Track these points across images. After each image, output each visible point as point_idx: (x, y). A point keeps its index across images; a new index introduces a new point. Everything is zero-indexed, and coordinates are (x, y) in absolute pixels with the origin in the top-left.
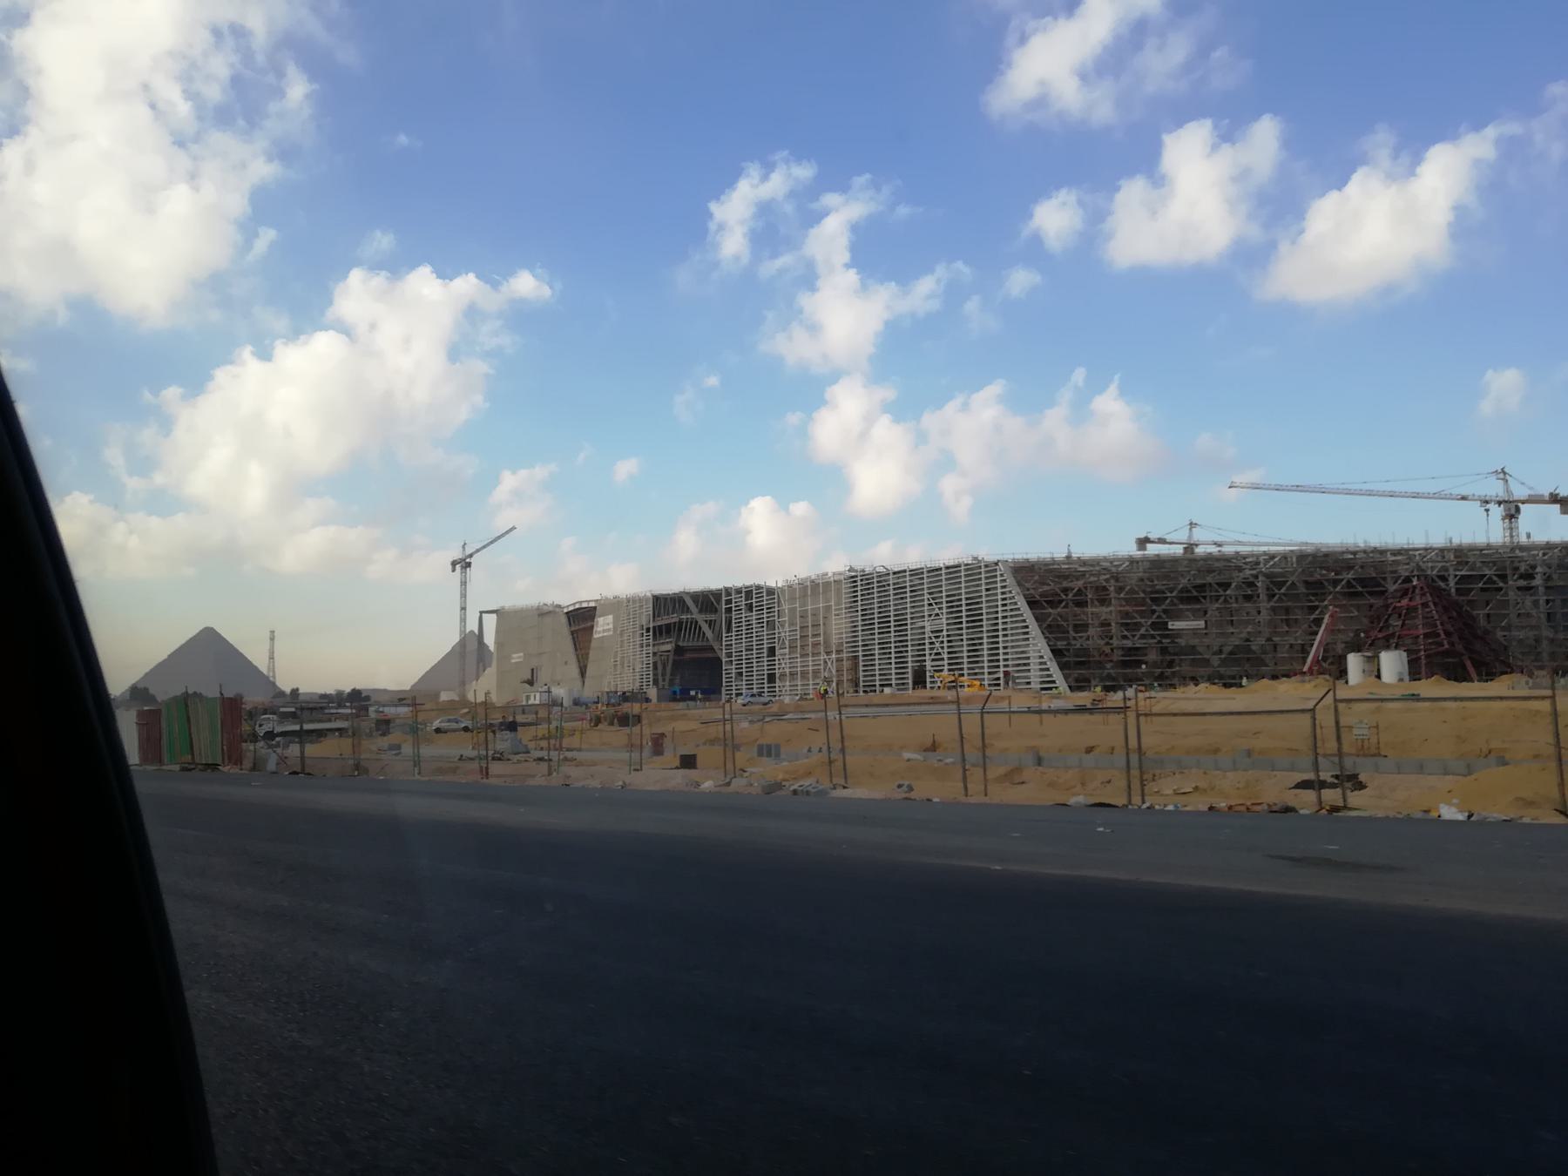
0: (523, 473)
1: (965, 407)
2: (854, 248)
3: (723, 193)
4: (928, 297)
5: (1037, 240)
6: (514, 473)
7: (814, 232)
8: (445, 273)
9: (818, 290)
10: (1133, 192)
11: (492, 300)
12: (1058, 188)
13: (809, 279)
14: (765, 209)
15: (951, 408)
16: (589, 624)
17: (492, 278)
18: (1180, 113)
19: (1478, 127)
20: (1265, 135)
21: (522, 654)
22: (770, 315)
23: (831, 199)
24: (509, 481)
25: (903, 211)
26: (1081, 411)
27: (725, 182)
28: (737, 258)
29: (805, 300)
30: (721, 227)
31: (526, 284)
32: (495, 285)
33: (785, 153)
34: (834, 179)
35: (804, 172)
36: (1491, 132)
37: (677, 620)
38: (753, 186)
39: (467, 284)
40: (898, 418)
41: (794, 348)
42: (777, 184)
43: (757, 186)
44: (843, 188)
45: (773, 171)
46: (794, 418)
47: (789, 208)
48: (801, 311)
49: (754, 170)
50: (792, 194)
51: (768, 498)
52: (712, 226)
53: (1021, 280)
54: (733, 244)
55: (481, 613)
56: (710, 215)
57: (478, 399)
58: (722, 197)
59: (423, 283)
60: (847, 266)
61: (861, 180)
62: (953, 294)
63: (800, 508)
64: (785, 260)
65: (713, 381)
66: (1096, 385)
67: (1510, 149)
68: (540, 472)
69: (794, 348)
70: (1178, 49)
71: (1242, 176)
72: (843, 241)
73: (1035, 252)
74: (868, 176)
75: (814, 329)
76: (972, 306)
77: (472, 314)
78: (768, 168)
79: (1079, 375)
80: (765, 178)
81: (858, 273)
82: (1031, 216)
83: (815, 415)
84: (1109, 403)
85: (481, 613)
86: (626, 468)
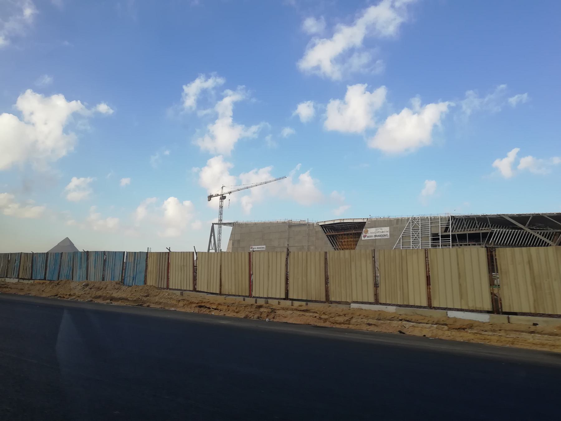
0: (82, 179)
1: (257, 173)
2: (234, 111)
3: (189, 83)
4: (254, 133)
5: (298, 117)
6: (78, 178)
7: (219, 102)
8: (69, 99)
9: (215, 124)
10: (333, 105)
11: (87, 113)
12: (307, 100)
13: (214, 118)
14: (204, 92)
15: (251, 173)
16: (360, 231)
17: (91, 103)
18: (357, 79)
19: (444, 101)
20: (381, 93)
21: (265, 246)
22: (198, 130)
23: (229, 92)
24: (75, 181)
25: (254, 100)
26: (296, 180)
27: (191, 79)
28: (191, 108)
29: (210, 127)
30: (187, 95)
31: (103, 108)
32: (88, 108)
33: (216, 73)
34: (231, 85)
35: (221, 81)
36: (447, 103)
37: (489, 231)
38: (201, 83)
39: (76, 105)
40: (231, 174)
41: (205, 144)
42: (210, 83)
43: (201, 83)
44: (234, 89)
45: (210, 78)
46: (195, 169)
47: (213, 93)
48: (209, 131)
49: (202, 77)
50: (214, 88)
51: (176, 199)
52: (183, 94)
53: (287, 131)
54: (190, 102)
55: (213, 224)
56: (183, 90)
57: (72, 148)
58: (188, 85)
59: (59, 101)
60: (231, 117)
61: (240, 87)
62: (263, 133)
63: (187, 203)
64: (208, 111)
65: (167, 153)
66: (303, 171)
67: (453, 110)
68: (89, 180)
69: (205, 144)
70: (365, 58)
71: (371, 105)
72: (231, 108)
73: (296, 122)
74: (244, 86)
75: (213, 138)
76: (268, 138)
77: (75, 115)
78: (208, 77)
79: (299, 166)
80: (206, 81)
81: (233, 120)
82: (296, 108)
83: (202, 169)
84: (306, 178)
85: (213, 224)
86: (125, 181)
